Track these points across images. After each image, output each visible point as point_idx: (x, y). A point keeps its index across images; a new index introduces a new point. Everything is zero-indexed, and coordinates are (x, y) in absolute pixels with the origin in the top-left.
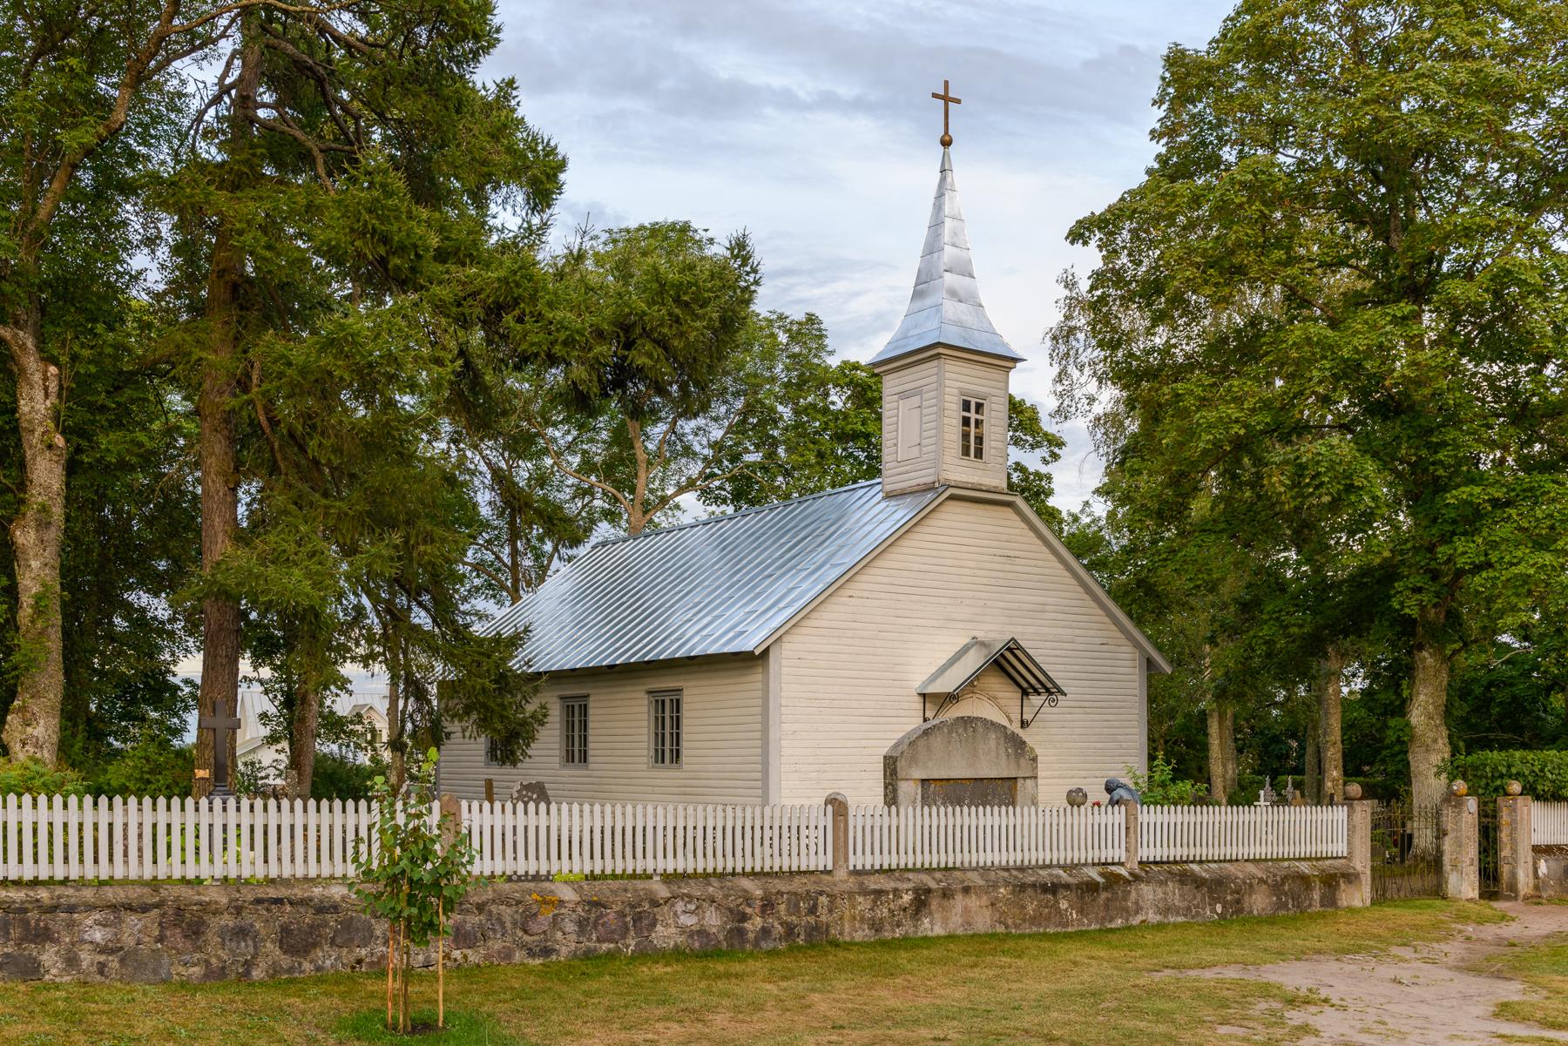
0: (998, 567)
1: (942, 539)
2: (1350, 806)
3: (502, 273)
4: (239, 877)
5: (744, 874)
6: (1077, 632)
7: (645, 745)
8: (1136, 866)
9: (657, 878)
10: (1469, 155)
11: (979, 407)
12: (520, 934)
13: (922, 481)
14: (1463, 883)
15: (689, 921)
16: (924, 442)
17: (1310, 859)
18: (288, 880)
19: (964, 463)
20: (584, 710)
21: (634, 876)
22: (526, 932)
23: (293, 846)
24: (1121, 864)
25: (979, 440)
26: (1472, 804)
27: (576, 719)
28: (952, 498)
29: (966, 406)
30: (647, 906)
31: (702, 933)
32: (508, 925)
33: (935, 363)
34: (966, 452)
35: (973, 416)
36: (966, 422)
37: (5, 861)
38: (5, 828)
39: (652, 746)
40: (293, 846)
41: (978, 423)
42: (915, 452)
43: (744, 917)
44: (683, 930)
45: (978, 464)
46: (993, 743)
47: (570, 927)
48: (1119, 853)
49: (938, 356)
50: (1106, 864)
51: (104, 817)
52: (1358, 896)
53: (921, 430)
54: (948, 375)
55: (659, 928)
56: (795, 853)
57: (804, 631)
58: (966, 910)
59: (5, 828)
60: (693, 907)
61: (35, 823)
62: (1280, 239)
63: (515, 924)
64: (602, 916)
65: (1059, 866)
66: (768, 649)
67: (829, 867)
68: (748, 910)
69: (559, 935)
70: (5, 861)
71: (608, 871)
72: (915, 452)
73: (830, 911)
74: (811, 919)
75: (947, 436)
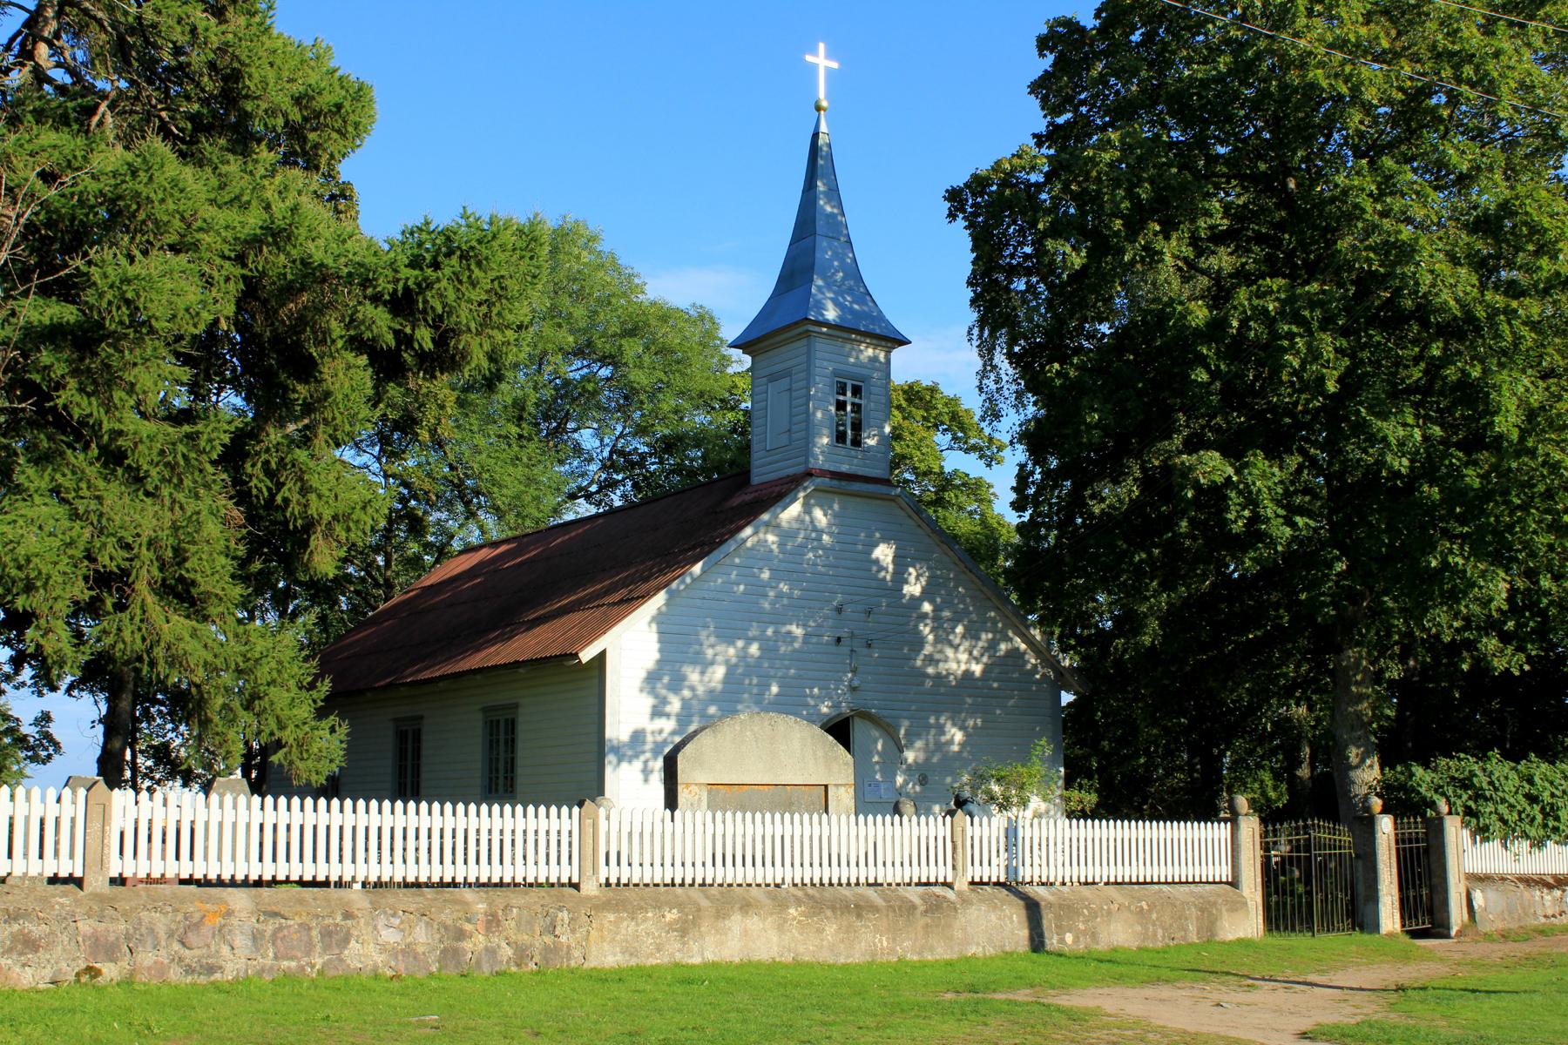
4: (25, 874)
5: (467, 884)
8: (965, 887)
9: (357, 886)
10: (1246, 100)
12: (176, 946)
14: (1389, 916)
15: (390, 936)
22: (183, 944)
23: (673, 848)
27: (502, 737)
29: (842, 390)
30: (339, 919)
31: (408, 951)
32: (162, 935)
37: (10, 856)
38: (11, 825)
40: (673, 848)
42: (784, 439)
43: (461, 935)
44: (383, 949)
47: (241, 941)
48: (943, 872)
50: (928, 884)
51: (425, 821)
53: (791, 416)
54: (818, 354)
55: (353, 943)
56: (807, 864)
58: (745, 933)
59: (11, 825)
61: (193, 822)
62: (1167, 200)
63: (171, 935)
67: (575, 880)
68: (468, 927)
69: (225, 950)
70: (10, 856)
74: (548, 939)
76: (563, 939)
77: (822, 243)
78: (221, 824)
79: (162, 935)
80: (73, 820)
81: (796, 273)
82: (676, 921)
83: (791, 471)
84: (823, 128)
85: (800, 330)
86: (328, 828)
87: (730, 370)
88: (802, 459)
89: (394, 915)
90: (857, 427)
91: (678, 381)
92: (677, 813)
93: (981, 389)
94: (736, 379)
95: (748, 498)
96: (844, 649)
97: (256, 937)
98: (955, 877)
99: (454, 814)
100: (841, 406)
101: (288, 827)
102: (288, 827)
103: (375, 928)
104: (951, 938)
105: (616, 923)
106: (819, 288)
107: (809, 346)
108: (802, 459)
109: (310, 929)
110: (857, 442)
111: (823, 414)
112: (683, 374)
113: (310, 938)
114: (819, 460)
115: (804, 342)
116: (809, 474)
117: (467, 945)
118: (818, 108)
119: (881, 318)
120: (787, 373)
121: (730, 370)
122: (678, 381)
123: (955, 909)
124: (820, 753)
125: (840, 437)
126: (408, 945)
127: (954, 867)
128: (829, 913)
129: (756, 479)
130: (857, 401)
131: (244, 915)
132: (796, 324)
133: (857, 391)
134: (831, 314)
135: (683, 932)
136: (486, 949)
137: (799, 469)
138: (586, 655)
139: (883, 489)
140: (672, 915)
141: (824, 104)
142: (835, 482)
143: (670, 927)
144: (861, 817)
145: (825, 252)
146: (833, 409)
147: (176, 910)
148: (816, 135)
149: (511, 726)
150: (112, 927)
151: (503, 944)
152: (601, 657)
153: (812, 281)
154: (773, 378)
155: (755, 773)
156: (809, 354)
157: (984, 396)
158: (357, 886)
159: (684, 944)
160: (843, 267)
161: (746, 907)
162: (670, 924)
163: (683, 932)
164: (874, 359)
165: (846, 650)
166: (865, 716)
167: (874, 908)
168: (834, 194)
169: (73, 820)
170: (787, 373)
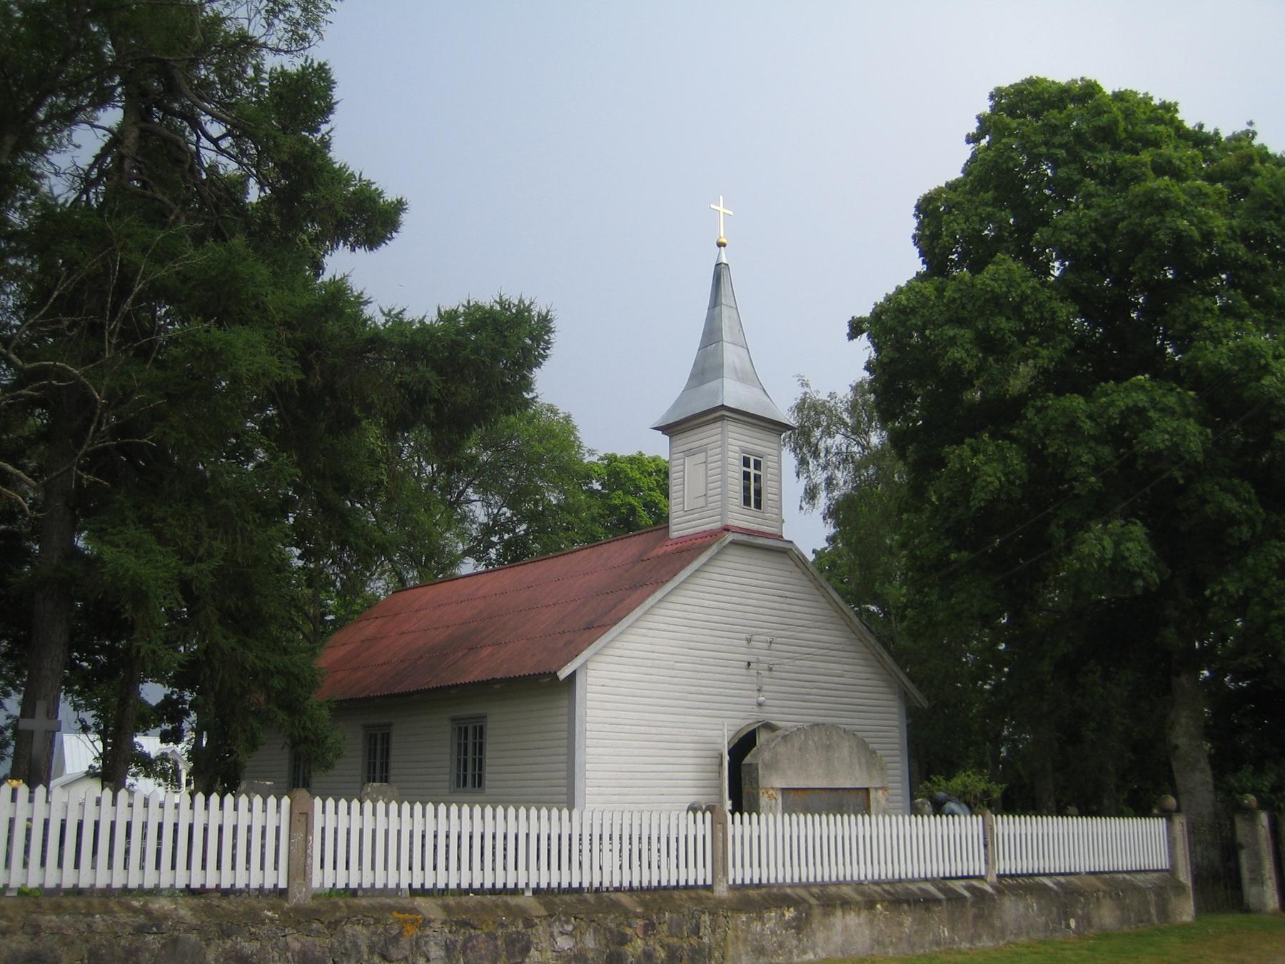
0: (776, 605)
1: (728, 578)
2: (1170, 819)
3: (217, 562)
6: (846, 667)
7: (447, 770)
11: (758, 465)
13: (707, 527)
15: (564, 943)
16: (710, 493)
17: (963, 878)
18: (241, 891)
19: (746, 511)
20: (386, 739)
21: (505, 890)
24: (981, 878)
25: (758, 493)
26: (1264, 818)
27: (379, 747)
28: (733, 543)
29: (746, 462)
33: (719, 424)
34: (747, 501)
35: (752, 471)
36: (746, 476)
39: (455, 771)
41: (757, 478)
42: (701, 502)
45: (758, 513)
46: (846, 752)
48: (978, 867)
49: (722, 418)
52: (1186, 910)
55: (533, 952)
57: (603, 658)
58: (846, 928)
60: (570, 928)
63: (372, 950)
64: (471, 938)
65: (926, 879)
66: (574, 672)
67: (709, 882)
68: (629, 931)
71: (453, 885)
72: (701, 502)
73: (713, 931)
74: (694, 940)
75: (730, 487)
76: (706, 940)
78: (374, 831)
79: (364, 949)
80: (278, 829)
82: (794, 919)
85: (717, 414)
86: (97, 824)
89: (568, 922)
92: (575, 813)
95: (670, 549)
96: (753, 672)
97: (449, 948)
98: (987, 872)
99: (207, 806)
101: (249, 829)
102: (249, 829)
103: (552, 935)
104: (992, 926)
105: (748, 924)
109: (496, 938)
113: (496, 947)
117: (629, 949)
120: (703, 449)
123: (994, 900)
124: (863, 760)
126: (580, 950)
127: (986, 862)
128: (905, 906)
129: (674, 534)
131: (437, 925)
135: (799, 929)
136: (645, 952)
138: (563, 674)
140: (790, 914)
143: (788, 926)
144: (786, 816)
145: (730, 355)
147: (377, 921)
149: (480, 732)
150: (318, 941)
151: (658, 947)
152: (573, 676)
155: (817, 780)
158: (529, 894)
159: (800, 940)
161: (846, 904)
162: (788, 922)
163: (799, 929)
165: (753, 672)
166: (769, 727)
167: (937, 901)
169: (278, 829)
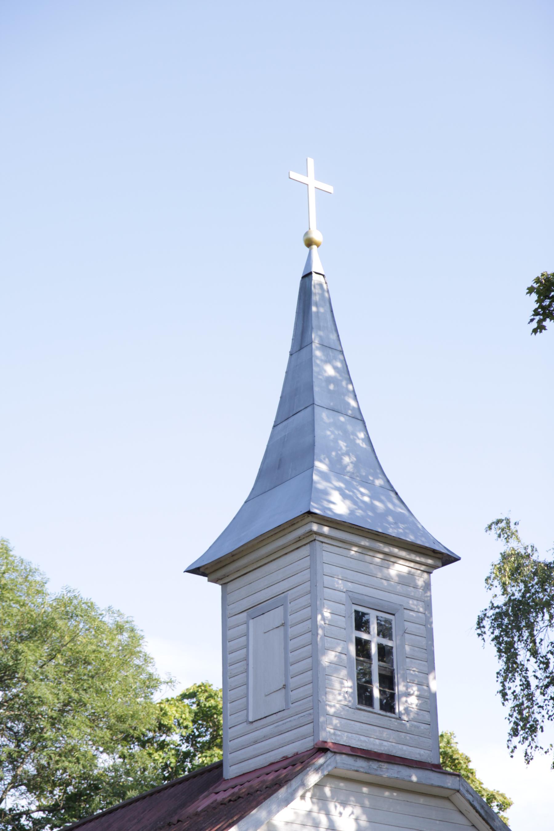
29: (361, 623)
53: (287, 664)
77: (323, 417)
81: (288, 456)
83: (289, 750)
84: (316, 267)
87: (157, 697)
88: (308, 729)
90: (388, 681)
91: (94, 702)
93: (504, 695)
94: (165, 706)
95: (220, 797)
100: (362, 647)
106: (325, 477)
107: (312, 556)
108: (308, 729)
110: (388, 705)
111: (337, 657)
112: (98, 692)
114: (329, 733)
115: (305, 551)
116: (322, 750)
118: (309, 243)
119: (408, 518)
120: (279, 601)
121: (157, 697)
122: (94, 702)
125: (364, 695)
130: (386, 642)
132: (292, 524)
133: (385, 631)
134: (340, 507)
137: (307, 744)
139: (434, 778)
141: (316, 236)
142: (361, 764)
146: (352, 649)
148: (307, 276)
153: (312, 467)
154: (256, 611)
156: (312, 568)
157: (510, 704)
160: (353, 448)
164: (406, 581)
168: (335, 350)
170: (279, 601)
